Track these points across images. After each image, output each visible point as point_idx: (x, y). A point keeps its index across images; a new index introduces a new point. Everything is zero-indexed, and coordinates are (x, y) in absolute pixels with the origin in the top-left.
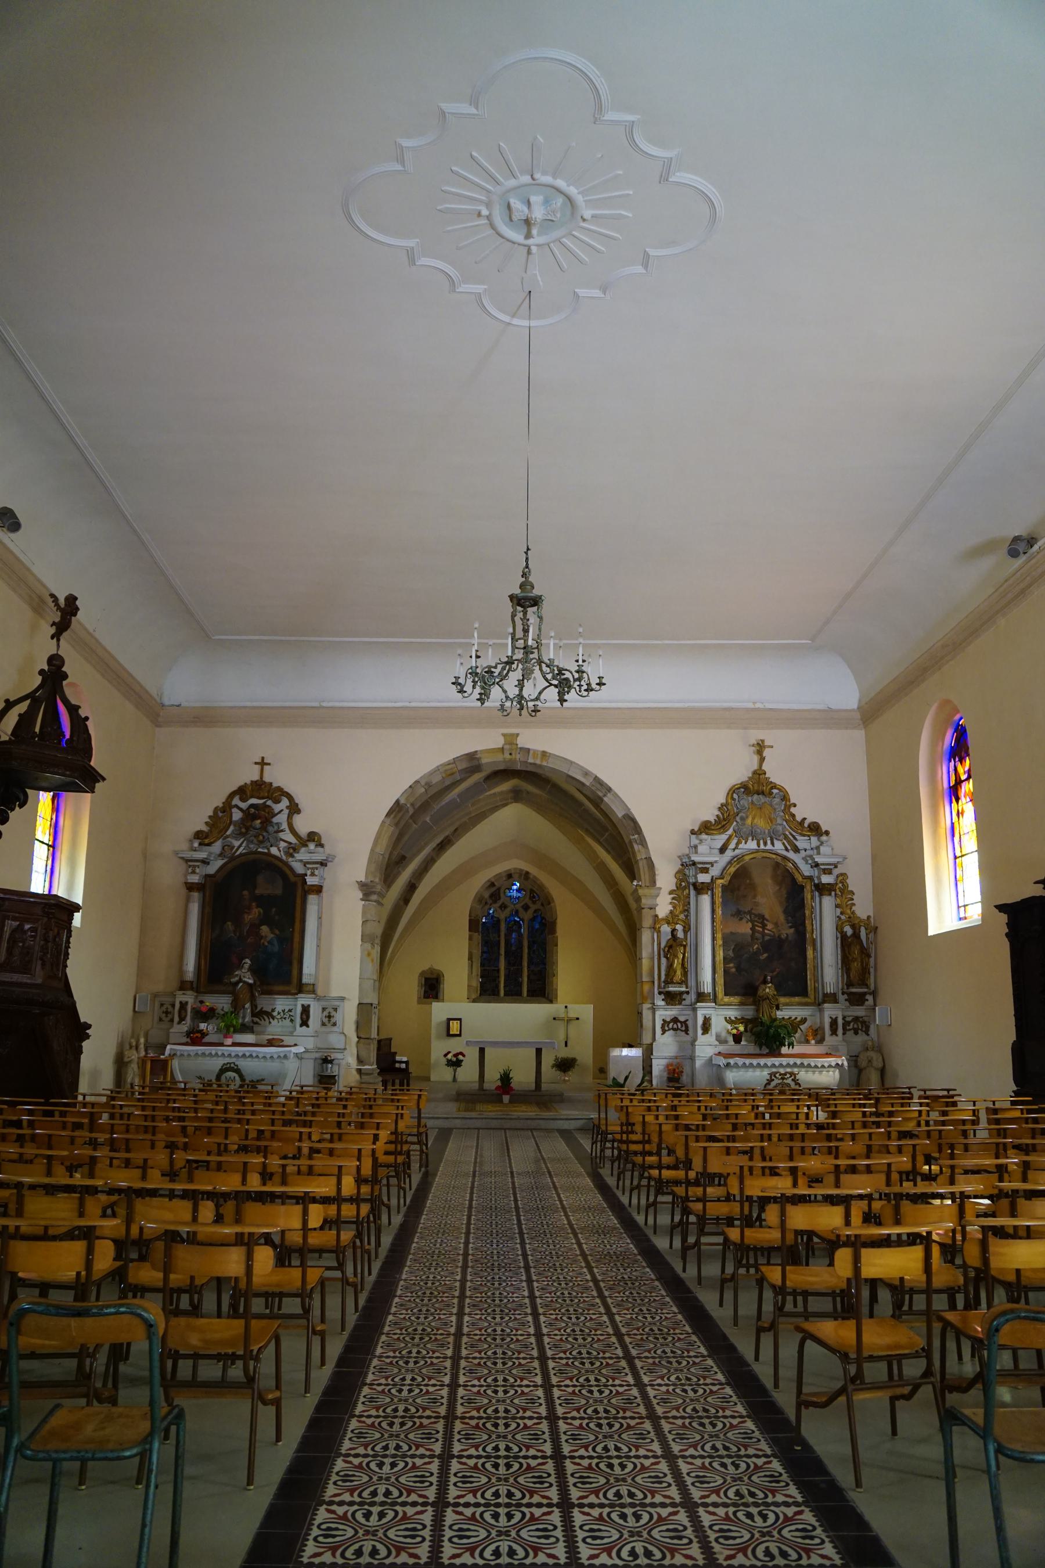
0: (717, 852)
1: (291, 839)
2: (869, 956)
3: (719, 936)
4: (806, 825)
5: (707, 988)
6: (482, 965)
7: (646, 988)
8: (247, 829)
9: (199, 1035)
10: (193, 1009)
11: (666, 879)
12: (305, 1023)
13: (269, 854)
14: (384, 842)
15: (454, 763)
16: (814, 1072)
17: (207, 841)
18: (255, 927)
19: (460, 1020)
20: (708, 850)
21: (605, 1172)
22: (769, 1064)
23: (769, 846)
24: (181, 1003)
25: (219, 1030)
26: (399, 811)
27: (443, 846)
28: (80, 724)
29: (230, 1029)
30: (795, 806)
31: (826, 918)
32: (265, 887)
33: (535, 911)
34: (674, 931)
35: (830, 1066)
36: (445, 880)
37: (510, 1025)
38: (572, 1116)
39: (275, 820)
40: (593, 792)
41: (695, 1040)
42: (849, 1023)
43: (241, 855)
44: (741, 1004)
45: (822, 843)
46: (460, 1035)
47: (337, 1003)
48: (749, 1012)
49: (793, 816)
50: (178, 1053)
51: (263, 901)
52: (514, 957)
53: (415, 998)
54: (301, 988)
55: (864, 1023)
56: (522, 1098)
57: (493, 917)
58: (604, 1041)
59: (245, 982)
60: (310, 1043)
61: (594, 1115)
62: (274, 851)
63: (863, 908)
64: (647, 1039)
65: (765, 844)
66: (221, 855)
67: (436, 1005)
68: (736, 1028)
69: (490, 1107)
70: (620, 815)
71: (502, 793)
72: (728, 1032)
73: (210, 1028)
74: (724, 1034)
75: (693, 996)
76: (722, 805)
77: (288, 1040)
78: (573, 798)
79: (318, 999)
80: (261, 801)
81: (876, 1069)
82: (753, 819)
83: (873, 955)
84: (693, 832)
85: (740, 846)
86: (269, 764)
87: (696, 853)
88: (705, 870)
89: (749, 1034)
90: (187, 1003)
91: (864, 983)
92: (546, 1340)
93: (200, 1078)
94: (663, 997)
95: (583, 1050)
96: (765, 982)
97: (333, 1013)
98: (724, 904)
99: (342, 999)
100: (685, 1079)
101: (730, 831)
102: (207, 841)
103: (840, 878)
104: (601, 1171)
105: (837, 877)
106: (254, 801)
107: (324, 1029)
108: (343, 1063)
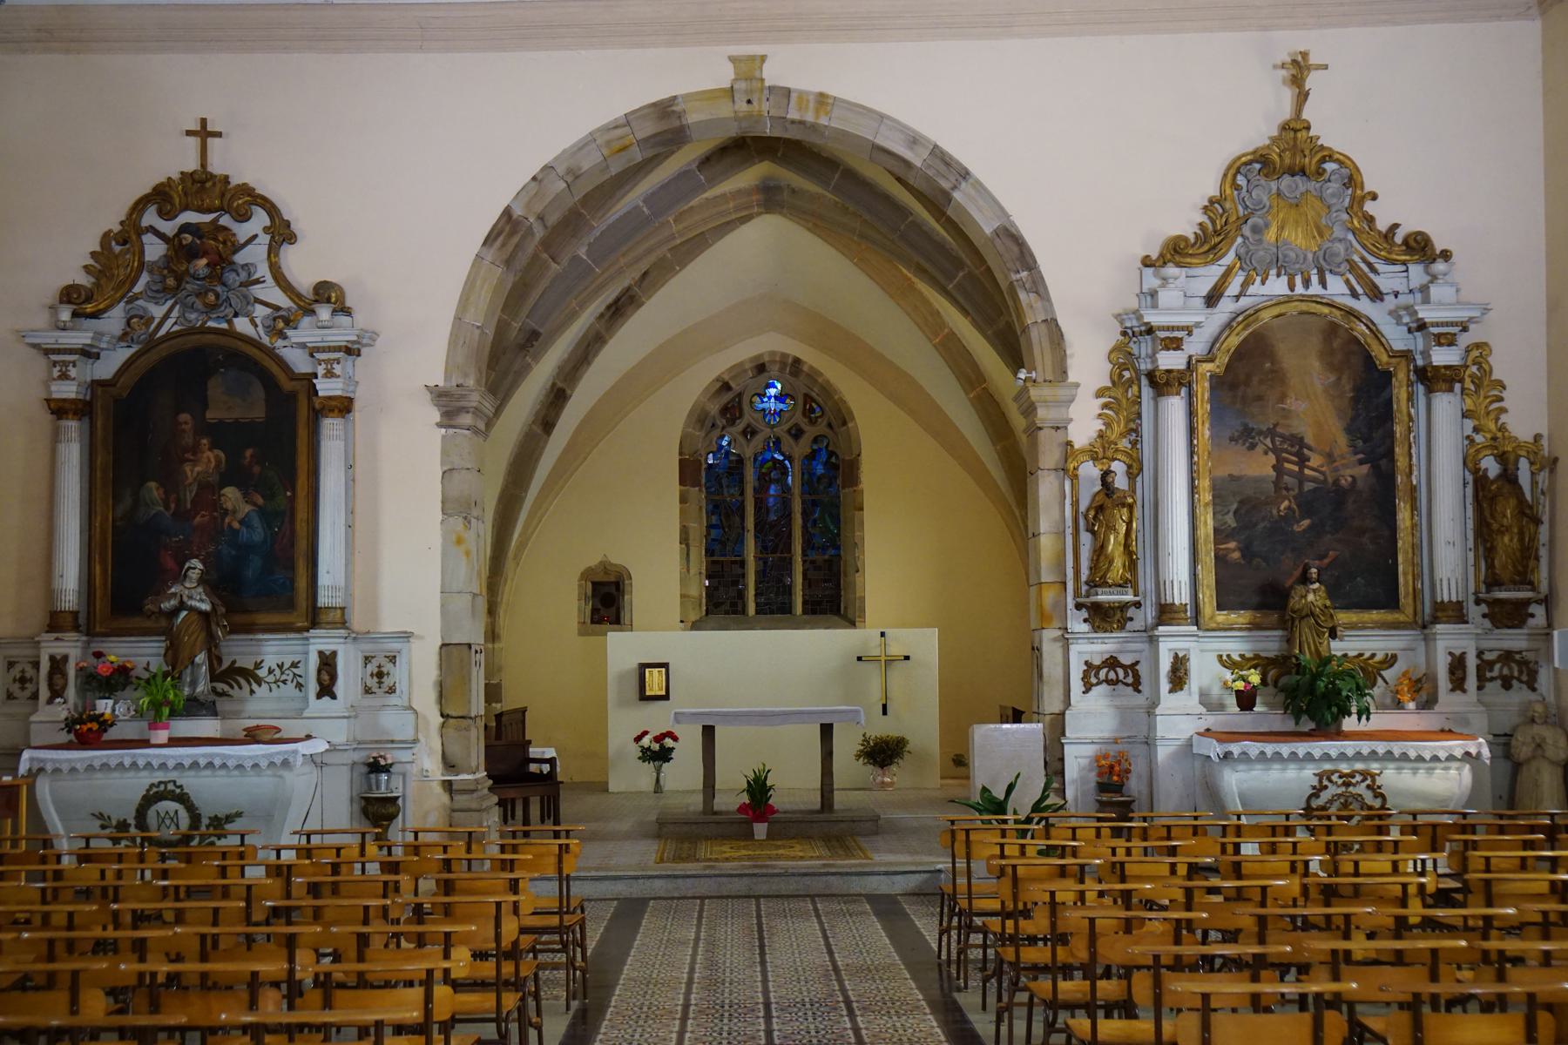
0: (1199, 303)
1: (281, 299)
2: (1537, 521)
3: (1204, 484)
4: (1398, 239)
6: (709, 552)
7: (1049, 596)
8: (179, 279)
9: (95, 726)
10: (80, 670)
11: (1089, 364)
13: (231, 334)
14: (484, 297)
15: (628, 123)
16: (1415, 771)
17: (89, 308)
18: (209, 491)
19: (665, 665)
20: (1181, 300)
21: (968, 1000)
22: (1317, 753)
23: (1315, 289)
24: (52, 658)
25: (139, 714)
26: (512, 233)
27: (619, 310)
30: (1374, 197)
31: (1439, 442)
32: (228, 403)
33: (815, 440)
34: (1106, 475)
35: (1451, 758)
36: (630, 378)
37: (763, 683)
38: (896, 865)
39: (240, 258)
40: (929, 179)
41: (1155, 703)
42: (1491, 664)
43: (169, 336)
44: (1255, 626)
45: (1434, 278)
46: (666, 697)
47: (395, 646)
48: (1271, 643)
49: (1370, 220)
50: (49, 767)
51: (219, 434)
52: (774, 537)
53: (574, 624)
54: (315, 618)
55: (1524, 664)
56: (794, 828)
57: (728, 453)
58: (963, 708)
59: (192, 609)
60: (340, 732)
61: (944, 864)
62: (242, 325)
63: (1525, 417)
64: (1052, 704)
65: (1307, 283)
68: (1243, 679)
69: (726, 849)
70: (988, 230)
71: (740, 192)
72: (1225, 686)
73: (121, 709)
74: (1216, 690)
75: (1149, 613)
76: (1211, 201)
77: (290, 728)
78: (887, 199)
80: (208, 218)
81: (1552, 763)
82: (1281, 228)
83: (1545, 518)
84: (1147, 262)
85: (1251, 290)
86: (219, 135)
87: (1155, 306)
88: (1175, 344)
89: (1271, 689)
90: (65, 658)
91: (1524, 578)
93: (101, 816)
94: (1084, 614)
95: (919, 722)
96: (1305, 579)
97: (388, 667)
98: (1217, 415)
99: (406, 636)
100: (1135, 786)
102: (89, 308)
103: (1475, 353)
104: (961, 998)
105: (1468, 351)
106: (190, 217)
107: (370, 701)
108: (414, 769)
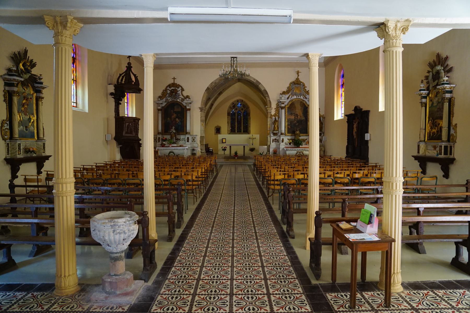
1: (183, 97)
5: (283, 132)
7: (269, 132)
11: (274, 105)
12: (188, 141)
27: (220, 94)
29: (171, 143)
32: (177, 109)
34: (275, 118)
37: (237, 140)
48: (293, 137)
51: (176, 112)
52: (239, 123)
54: (187, 133)
60: (189, 146)
62: (178, 100)
64: (269, 144)
66: (165, 102)
67: (219, 135)
75: (280, 134)
77: (184, 145)
79: (191, 135)
84: (281, 94)
88: (283, 104)
92: (258, 234)
98: (288, 112)
99: (197, 135)
100: (277, 153)
106: (172, 88)
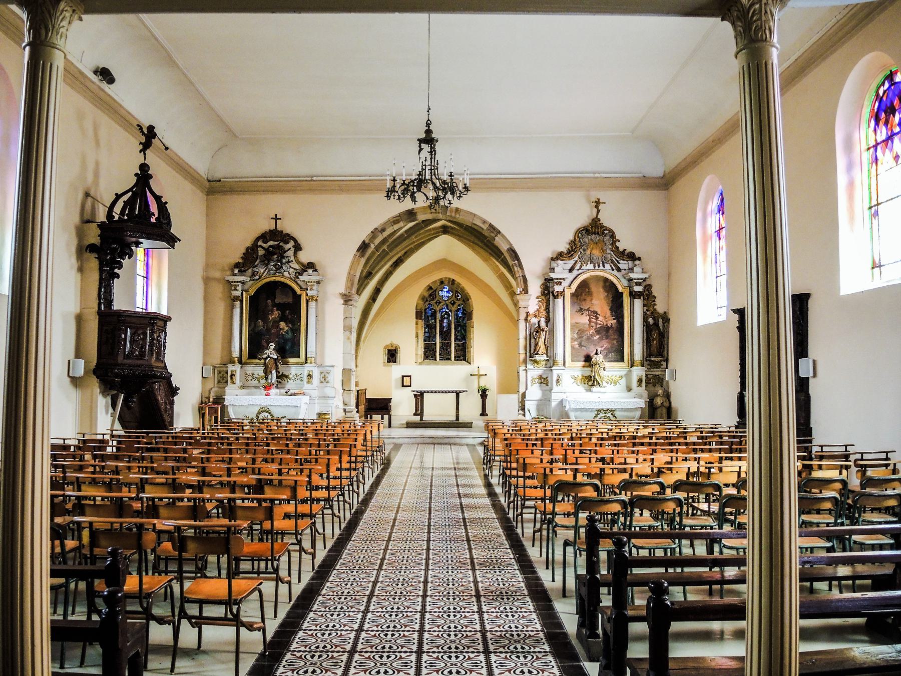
6: (425, 340)
18: (276, 323)
20: (561, 270)
28: (162, 207)
39: (286, 255)
45: (635, 266)
51: (281, 307)
52: (445, 335)
64: (522, 389)
65: (599, 266)
67: (394, 367)
80: (276, 243)
84: (552, 259)
88: (560, 284)
99: (333, 366)
101: (576, 258)
106: (271, 243)
